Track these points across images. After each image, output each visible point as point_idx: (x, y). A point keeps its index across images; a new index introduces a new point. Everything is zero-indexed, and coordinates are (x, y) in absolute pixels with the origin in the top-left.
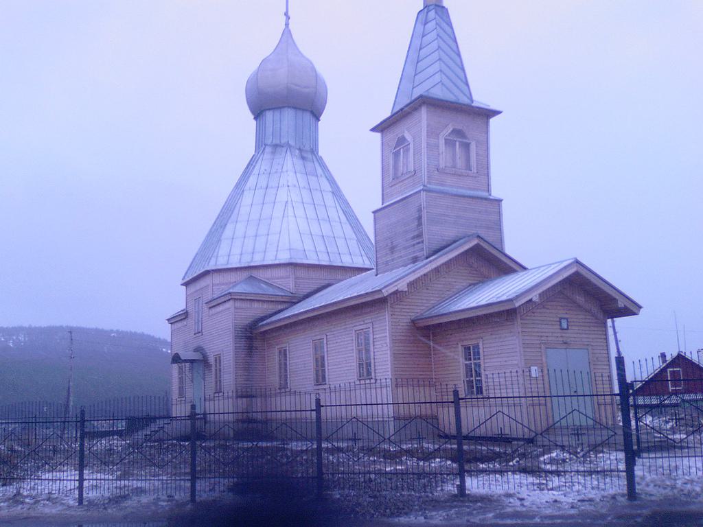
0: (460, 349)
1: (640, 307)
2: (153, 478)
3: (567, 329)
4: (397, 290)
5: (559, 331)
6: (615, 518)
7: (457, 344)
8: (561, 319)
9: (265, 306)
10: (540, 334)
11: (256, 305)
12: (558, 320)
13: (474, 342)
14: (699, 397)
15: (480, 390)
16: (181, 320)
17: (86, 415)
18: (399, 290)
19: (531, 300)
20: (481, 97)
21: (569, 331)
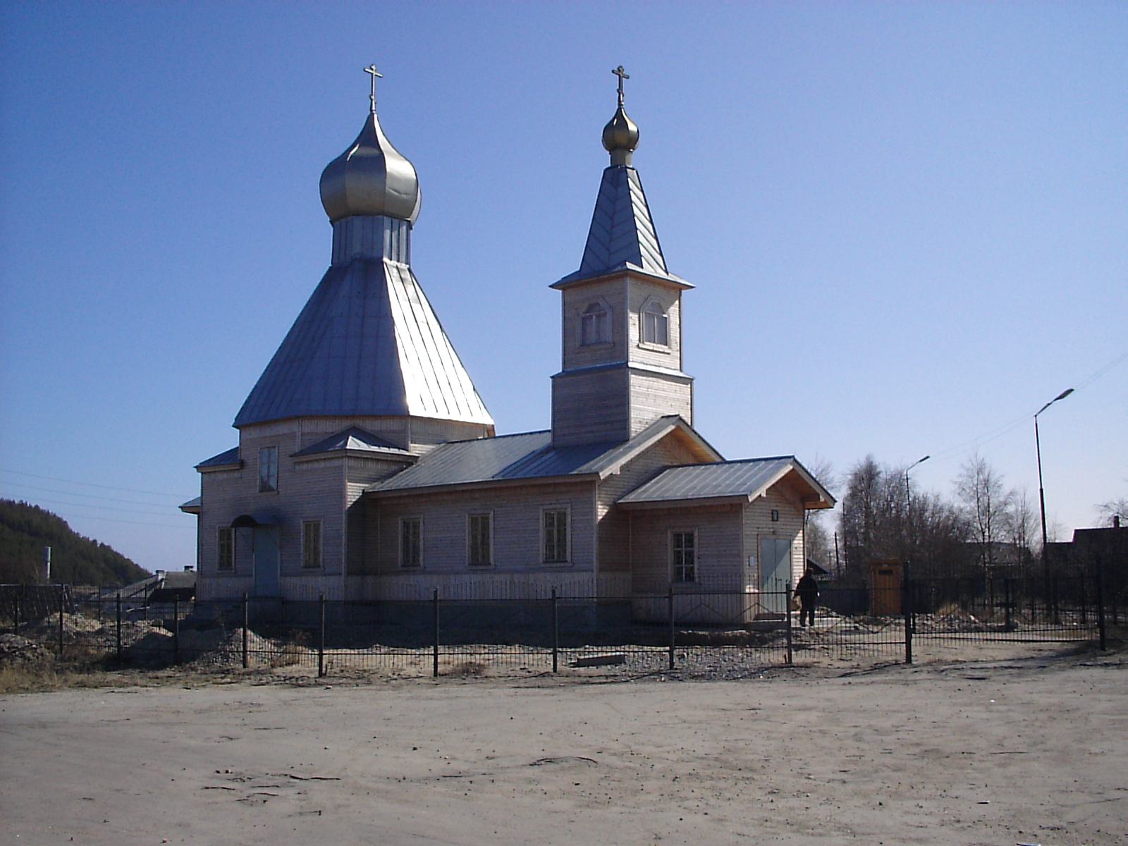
0: (670, 535)
1: (835, 501)
2: (626, 653)
3: (777, 521)
4: (611, 474)
5: (771, 522)
6: (1124, 643)
7: (539, 508)
8: (773, 510)
9: (379, 466)
10: (758, 526)
11: (370, 464)
12: (770, 512)
13: (688, 530)
14: (2, 585)
15: (690, 577)
16: (234, 470)
17: (556, 593)
18: (614, 473)
19: (760, 496)
20: (413, 227)
21: (778, 522)
